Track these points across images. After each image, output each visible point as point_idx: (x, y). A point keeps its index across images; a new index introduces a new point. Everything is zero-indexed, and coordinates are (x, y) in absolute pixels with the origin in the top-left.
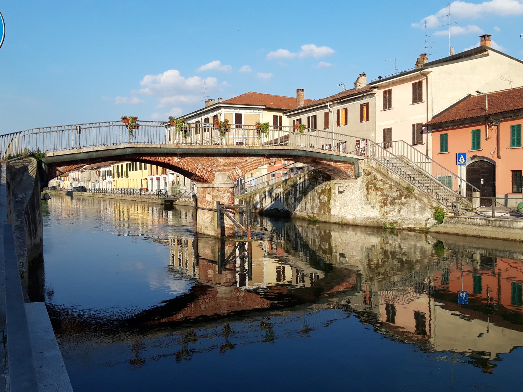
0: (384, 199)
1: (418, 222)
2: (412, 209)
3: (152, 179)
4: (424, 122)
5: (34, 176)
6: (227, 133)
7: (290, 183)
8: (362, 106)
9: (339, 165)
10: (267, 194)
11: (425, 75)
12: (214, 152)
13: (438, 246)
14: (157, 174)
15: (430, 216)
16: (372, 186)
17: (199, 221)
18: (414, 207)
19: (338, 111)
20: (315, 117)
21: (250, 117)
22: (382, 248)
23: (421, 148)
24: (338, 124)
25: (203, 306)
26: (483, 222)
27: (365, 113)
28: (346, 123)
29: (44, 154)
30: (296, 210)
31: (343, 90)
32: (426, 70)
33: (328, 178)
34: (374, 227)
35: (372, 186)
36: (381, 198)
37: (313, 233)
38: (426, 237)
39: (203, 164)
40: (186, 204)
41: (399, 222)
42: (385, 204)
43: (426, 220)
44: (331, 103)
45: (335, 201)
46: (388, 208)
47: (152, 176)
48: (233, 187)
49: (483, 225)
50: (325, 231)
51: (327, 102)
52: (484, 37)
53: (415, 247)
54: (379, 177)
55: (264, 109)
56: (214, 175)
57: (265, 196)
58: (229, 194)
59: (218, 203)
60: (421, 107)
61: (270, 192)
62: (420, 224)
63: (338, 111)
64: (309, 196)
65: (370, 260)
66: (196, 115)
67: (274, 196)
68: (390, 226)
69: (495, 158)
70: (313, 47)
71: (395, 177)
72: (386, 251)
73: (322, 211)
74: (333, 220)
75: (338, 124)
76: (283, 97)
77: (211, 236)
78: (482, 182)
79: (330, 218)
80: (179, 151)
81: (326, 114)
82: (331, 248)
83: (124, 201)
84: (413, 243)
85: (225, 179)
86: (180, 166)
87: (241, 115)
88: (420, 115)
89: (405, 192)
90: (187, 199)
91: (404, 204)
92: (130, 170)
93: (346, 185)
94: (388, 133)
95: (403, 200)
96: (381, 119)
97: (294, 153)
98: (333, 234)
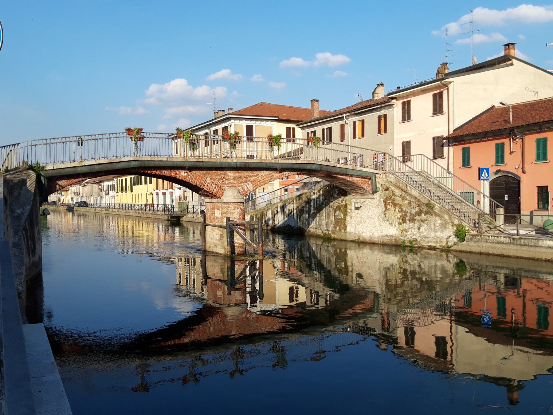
0: (403, 216)
2: (432, 226)
3: (157, 194)
4: (445, 135)
5: (33, 190)
6: (237, 145)
7: (304, 198)
8: (379, 117)
9: (355, 179)
10: (279, 210)
11: (446, 86)
12: (224, 166)
14: (163, 188)
15: (451, 234)
16: (390, 201)
17: (208, 238)
19: (355, 123)
20: (330, 129)
21: (262, 128)
23: (442, 162)
24: (355, 137)
25: (211, 329)
26: (507, 240)
27: (383, 125)
28: (363, 135)
29: (43, 167)
30: (310, 227)
31: (360, 101)
32: (447, 80)
33: (344, 193)
34: (392, 245)
35: (390, 201)
36: (399, 215)
37: (328, 251)
38: (447, 256)
39: (211, 178)
40: (194, 220)
41: (419, 240)
42: (404, 221)
44: (347, 114)
45: (351, 218)
46: (407, 225)
47: (158, 191)
48: (243, 203)
49: (507, 244)
50: (340, 250)
51: (343, 114)
52: (508, 46)
53: (436, 265)
54: (397, 192)
55: (276, 121)
57: (278, 212)
58: (239, 210)
59: (228, 219)
60: (442, 118)
61: (283, 208)
62: (441, 242)
63: (355, 123)
64: (324, 212)
65: (387, 281)
67: (287, 212)
68: (409, 244)
69: (519, 173)
70: (328, 55)
71: (415, 192)
72: (405, 270)
74: (349, 238)
75: (355, 137)
76: (297, 108)
77: (220, 254)
78: (506, 199)
79: (346, 235)
80: (187, 165)
81: (342, 126)
83: (128, 217)
84: (433, 262)
85: (236, 194)
86: (187, 180)
87: (252, 126)
88: (441, 127)
89: (425, 209)
90: (195, 215)
92: (134, 185)
94: (407, 146)
95: (423, 216)
96: (400, 133)
97: (308, 167)
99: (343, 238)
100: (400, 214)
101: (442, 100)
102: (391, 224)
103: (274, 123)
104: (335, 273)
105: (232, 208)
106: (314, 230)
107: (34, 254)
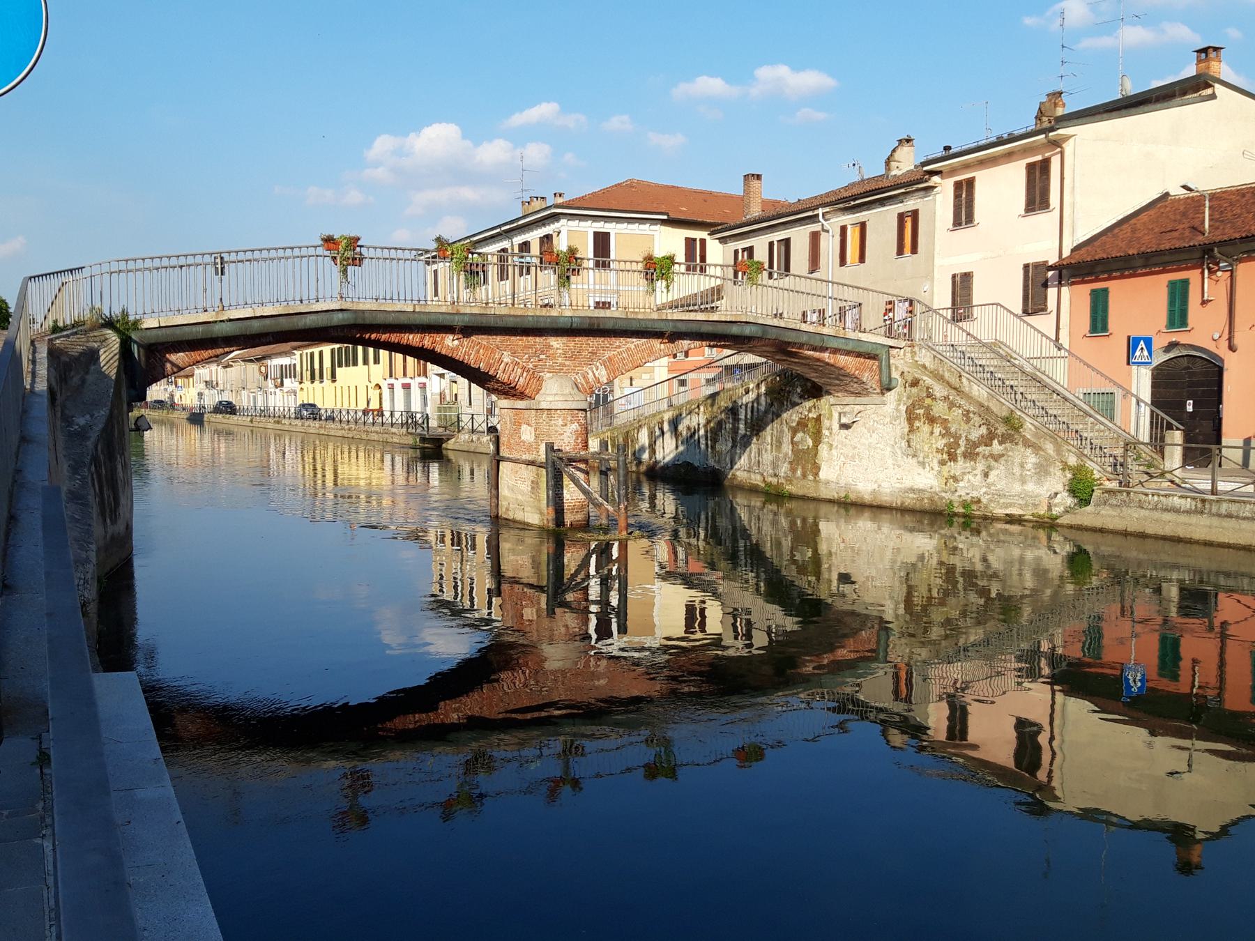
0: (949, 445)
1: (1030, 501)
2: (1017, 470)
3: (391, 387)
4: (1053, 260)
5: (113, 373)
6: (573, 278)
7: (723, 403)
8: (901, 217)
9: (842, 360)
10: (666, 427)
11: (1056, 144)
12: (542, 325)
13: (1078, 561)
14: (405, 375)
15: (1060, 487)
16: (921, 411)
17: (504, 491)
18: (1022, 466)
19: (843, 229)
20: (787, 242)
22: (941, 563)
23: (1044, 322)
24: (843, 262)
26: (1187, 504)
27: (909, 236)
28: (862, 259)
29: (136, 322)
30: (736, 467)
32: (1060, 131)
33: (815, 392)
34: (923, 512)
35: (921, 411)
36: (941, 443)
37: (775, 523)
38: (1049, 538)
39: (514, 353)
41: (984, 501)
42: (953, 457)
43: (1051, 498)
44: (827, 209)
46: (959, 466)
47: (392, 381)
48: (585, 410)
49: (1188, 512)
50: (804, 520)
51: (817, 208)
53: (1022, 560)
54: (939, 390)
55: (663, 222)
56: (540, 380)
57: (663, 433)
58: (575, 426)
59: (550, 447)
60: (1046, 221)
61: (674, 423)
62: (1035, 505)
63: (843, 229)
64: (768, 434)
66: (499, 235)
67: (684, 433)
68: (961, 510)
69: (1222, 351)
70: (783, 71)
71: (979, 392)
72: (951, 570)
73: (799, 473)
74: (825, 493)
75: (843, 262)
78: (1190, 409)
79: (817, 488)
80: (458, 321)
81: (815, 237)
82: (817, 560)
84: (1016, 552)
85: (568, 389)
86: (459, 356)
87: (607, 235)
88: (1044, 241)
89: (1001, 429)
90: (475, 437)
91: (997, 458)
92: (340, 366)
93: (857, 408)
94: (962, 285)
95: (996, 447)
96: (947, 250)
97: (735, 330)
98: (823, 526)
99: (812, 494)
100: (944, 441)
101: (1048, 179)
102: (922, 464)
103: (658, 227)
104: (789, 572)
105: (560, 422)
106: (745, 475)
107: (115, 518)
